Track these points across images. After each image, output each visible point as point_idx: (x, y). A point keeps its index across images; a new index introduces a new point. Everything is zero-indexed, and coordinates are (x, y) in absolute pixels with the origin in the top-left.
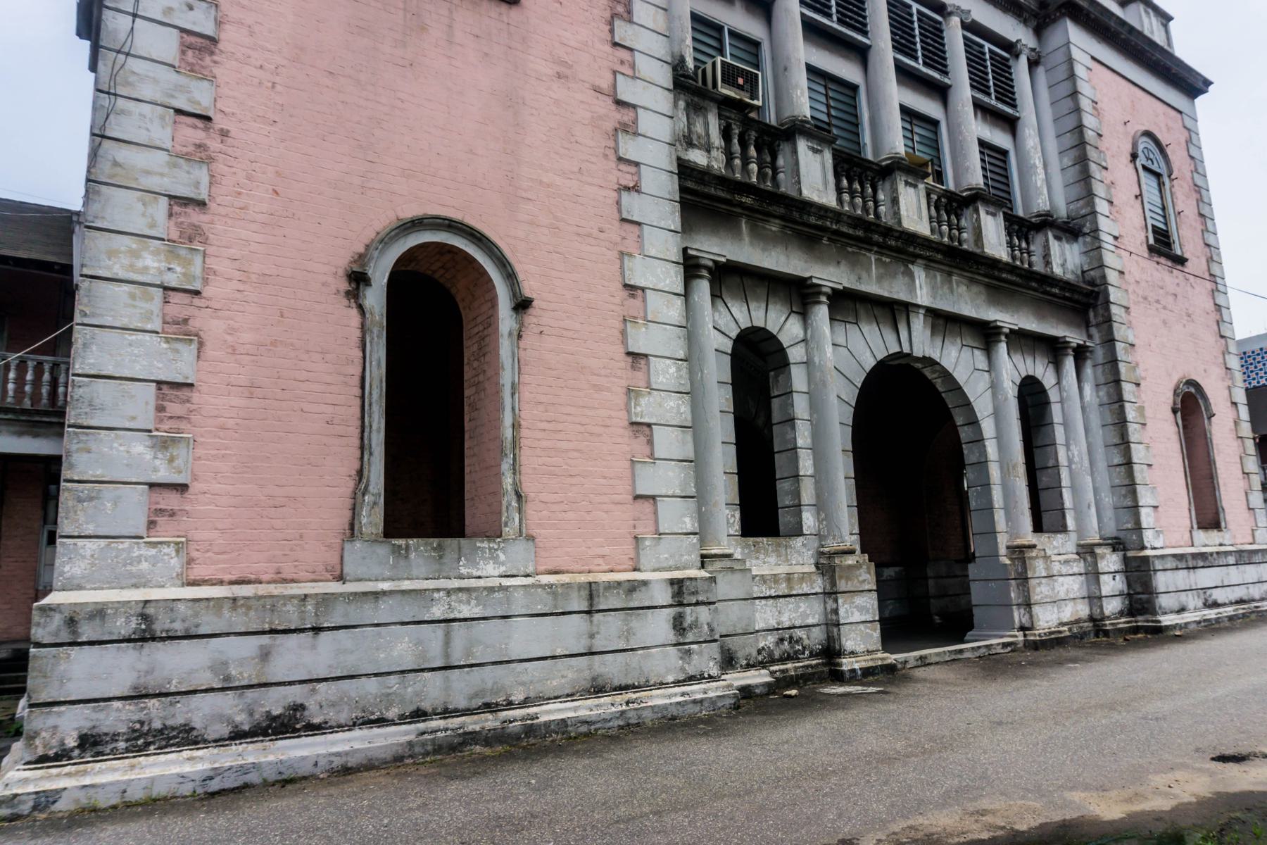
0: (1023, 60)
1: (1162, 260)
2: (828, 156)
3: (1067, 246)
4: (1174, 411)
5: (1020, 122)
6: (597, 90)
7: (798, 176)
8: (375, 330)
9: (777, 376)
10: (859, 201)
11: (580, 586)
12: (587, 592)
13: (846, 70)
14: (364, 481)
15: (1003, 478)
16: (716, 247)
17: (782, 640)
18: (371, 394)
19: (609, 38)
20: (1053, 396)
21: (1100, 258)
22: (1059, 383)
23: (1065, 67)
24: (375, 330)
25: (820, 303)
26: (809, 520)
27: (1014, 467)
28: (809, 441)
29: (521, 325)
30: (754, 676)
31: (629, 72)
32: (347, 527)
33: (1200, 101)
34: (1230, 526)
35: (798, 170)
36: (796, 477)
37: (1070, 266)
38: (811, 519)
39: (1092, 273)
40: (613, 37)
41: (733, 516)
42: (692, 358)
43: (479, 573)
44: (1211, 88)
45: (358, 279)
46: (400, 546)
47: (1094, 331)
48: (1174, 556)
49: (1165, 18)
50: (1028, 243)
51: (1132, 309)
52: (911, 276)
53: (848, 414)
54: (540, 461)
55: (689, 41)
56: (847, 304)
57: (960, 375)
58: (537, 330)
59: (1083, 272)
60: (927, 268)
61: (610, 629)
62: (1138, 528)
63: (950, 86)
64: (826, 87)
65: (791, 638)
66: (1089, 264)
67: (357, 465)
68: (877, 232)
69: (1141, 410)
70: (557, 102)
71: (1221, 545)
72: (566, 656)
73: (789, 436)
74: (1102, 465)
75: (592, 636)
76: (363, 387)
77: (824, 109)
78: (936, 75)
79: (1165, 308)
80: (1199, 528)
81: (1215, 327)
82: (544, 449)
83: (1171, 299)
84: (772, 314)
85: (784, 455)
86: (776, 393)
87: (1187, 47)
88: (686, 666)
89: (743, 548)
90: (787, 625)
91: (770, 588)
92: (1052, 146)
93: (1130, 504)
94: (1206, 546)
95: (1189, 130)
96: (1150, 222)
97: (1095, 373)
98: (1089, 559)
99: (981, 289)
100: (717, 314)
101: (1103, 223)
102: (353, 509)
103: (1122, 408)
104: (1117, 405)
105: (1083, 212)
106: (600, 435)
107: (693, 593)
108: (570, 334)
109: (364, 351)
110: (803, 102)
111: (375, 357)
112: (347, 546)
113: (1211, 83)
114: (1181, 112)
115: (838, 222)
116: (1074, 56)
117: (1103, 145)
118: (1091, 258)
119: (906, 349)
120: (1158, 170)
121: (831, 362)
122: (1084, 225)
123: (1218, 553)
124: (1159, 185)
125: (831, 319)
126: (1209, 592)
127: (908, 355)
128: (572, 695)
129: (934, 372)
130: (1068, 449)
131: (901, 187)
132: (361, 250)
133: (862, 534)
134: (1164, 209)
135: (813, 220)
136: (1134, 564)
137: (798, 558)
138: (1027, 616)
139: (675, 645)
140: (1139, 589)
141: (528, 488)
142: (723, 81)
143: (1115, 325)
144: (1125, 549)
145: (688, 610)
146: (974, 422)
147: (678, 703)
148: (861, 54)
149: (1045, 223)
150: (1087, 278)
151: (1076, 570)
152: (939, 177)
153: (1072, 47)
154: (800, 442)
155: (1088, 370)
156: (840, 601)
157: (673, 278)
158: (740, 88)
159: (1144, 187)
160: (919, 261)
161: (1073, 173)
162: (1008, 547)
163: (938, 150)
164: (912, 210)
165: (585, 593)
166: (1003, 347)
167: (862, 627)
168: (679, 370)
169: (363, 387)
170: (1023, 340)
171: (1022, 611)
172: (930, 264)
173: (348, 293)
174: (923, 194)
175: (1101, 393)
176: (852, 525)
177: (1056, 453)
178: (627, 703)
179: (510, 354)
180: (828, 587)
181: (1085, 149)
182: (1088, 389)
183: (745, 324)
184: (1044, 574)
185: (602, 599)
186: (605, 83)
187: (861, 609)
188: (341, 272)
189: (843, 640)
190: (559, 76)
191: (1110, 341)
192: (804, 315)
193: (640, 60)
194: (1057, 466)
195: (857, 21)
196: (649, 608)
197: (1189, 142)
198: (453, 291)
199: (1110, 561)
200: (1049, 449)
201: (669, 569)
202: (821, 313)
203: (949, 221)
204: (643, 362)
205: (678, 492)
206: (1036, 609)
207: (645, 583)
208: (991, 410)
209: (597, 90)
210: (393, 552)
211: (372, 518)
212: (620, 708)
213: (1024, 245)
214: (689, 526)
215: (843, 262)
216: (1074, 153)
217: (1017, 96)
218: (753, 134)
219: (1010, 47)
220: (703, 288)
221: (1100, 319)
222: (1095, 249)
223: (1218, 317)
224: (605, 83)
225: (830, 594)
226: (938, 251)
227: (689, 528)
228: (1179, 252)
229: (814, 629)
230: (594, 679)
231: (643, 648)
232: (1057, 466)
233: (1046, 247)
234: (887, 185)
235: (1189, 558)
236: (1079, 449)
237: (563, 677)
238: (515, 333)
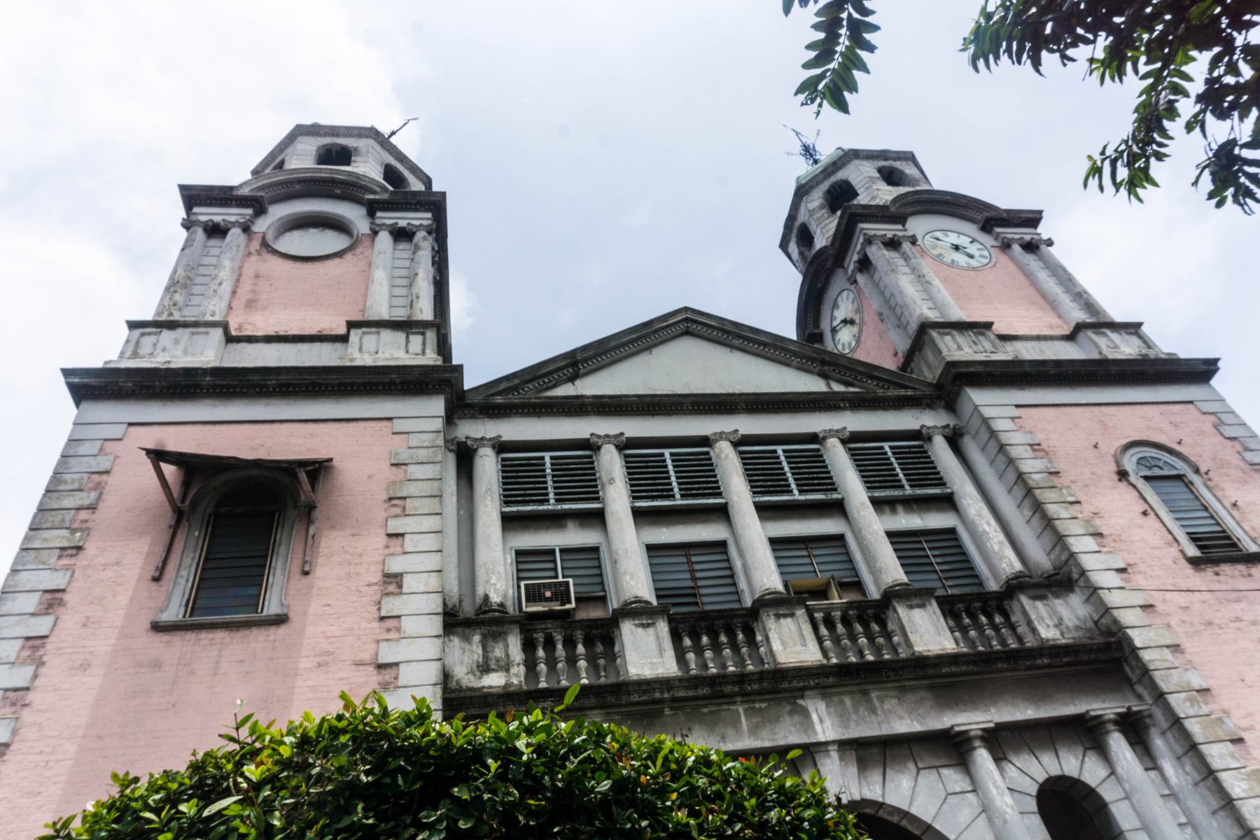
5: (956, 496)
20: (1109, 793)
23: (983, 429)
33: (1214, 382)
39: (1103, 621)
44: (1220, 364)
47: (1139, 689)
49: (1133, 328)
51: (1187, 644)
52: (805, 713)
59: (1096, 623)
60: (824, 696)
63: (952, 493)
66: (1096, 611)
68: (727, 683)
70: (313, 688)
87: (1172, 340)
97: (1167, 741)
99: (923, 694)
105: (1064, 557)
113: (1217, 360)
114: (1191, 402)
115: (669, 689)
116: (986, 415)
118: (1093, 604)
120: (1174, 472)
124: (1187, 486)
134: (1206, 509)
135: (635, 698)
155: (1158, 743)
158: (547, 600)
160: (807, 693)
172: (824, 692)
181: (1033, 495)
183: (1041, 777)
191: (1160, 697)
202: (982, 758)
216: (1027, 503)
218: (579, 635)
221: (1138, 672)
222: (1093, 592)
226: (827, 676)
233: (1025, 613)
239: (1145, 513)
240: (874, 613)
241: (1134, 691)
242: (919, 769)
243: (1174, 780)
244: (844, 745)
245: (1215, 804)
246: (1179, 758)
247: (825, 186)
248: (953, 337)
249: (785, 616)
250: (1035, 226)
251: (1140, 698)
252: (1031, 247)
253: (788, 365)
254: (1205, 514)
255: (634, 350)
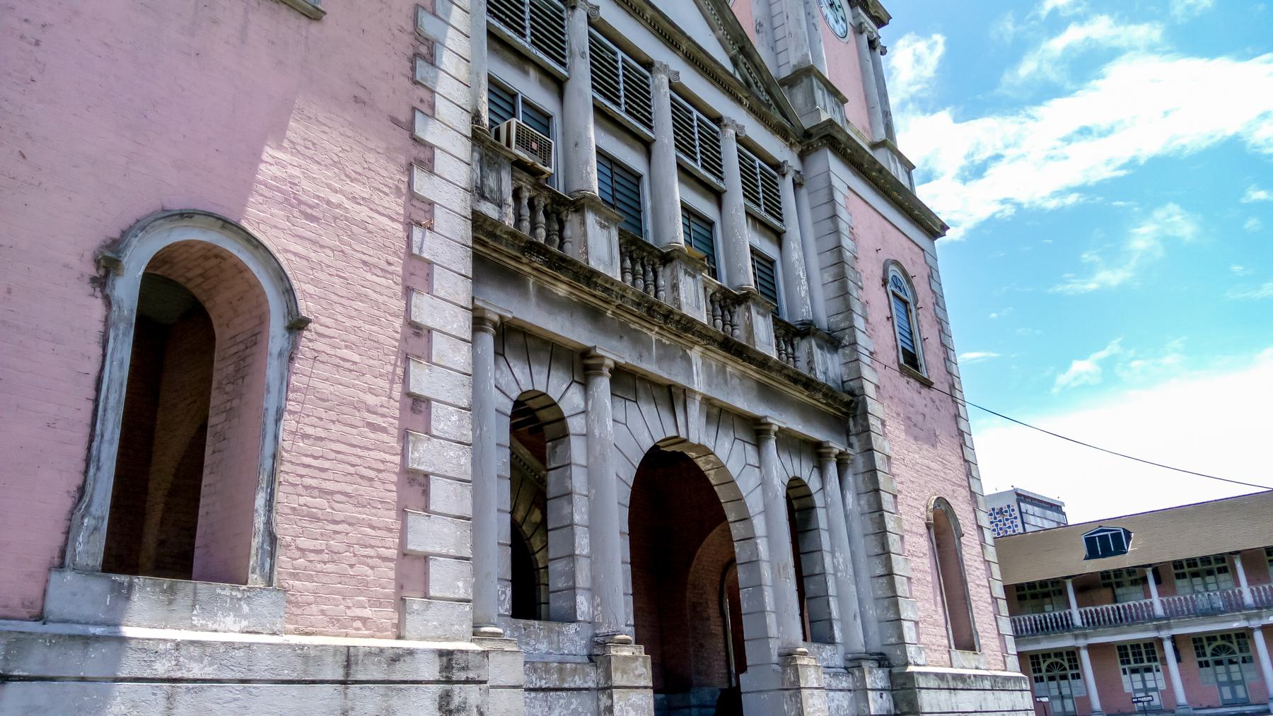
0: (789, 179)
1: (912, 380)
2: (614, 233)
3: (828, 356)
4: (928, 526)
6: (395, 121)
7: (586, 247)
8: (122, 326)
9: (554, 447)
10: (640, 282)
11: (336, 649)
12: (344, 658)
13: (631, 158)
14: (86, 499)
15: (773, 580)
16: (504, 304)
18: (107, 397)
20: (818, 500)
22: (823, 488)
23: (825, 191)
24: (122, 326)
25: (601, 375)
26: (583, 605)
27: (785, 567)
29: (294, 346)
31: (428, 111)
32: (56, 553)
33: (938, 242)
35: (586, 241)
36: (572, 556)
37: (831, 374)
38: (585, 604)
41: (504, 592)
42: (475, 408)
43: (215, 626)
44: (947, 232)
45: (107, 265)
46: (121, 584)
47: (853, 439)
48: (936, 674)
49: (909, 167)
53: (625, 495)
54: (302, 500)
57: (734, 468)
58: (309, 354)
59: (843, 382)
62: (901, 642)
67: (79, 481)
73: (566, 511)
74: (864, 575)
76: (98, 389)
80: (957, 648)
82: (306, 487)
83: (920, 418)
85: (557, 532)
86: (553, 465)
92: (815, 263)
98: (857, 673)
100: (498, 373)
101: (861, 339)
102: (68, 533)
106: (371, 479)
107: (463, 669)
108: (347, 365)
109: (104, 347)
110: (592, 181)
111: (118, 356)
112: (55, 577)
119: (683, 435)
121: (609, 441)
122: (843, 338)
123: (975, 676)
127: (684, 441)
129: (707, 462)
130: (833, 556)
131: (681, 274)
132: (117, 235)
134: (911, 334)
136: (900, 681)
137: (573, 640)
141: (284, 529)
142: (517, 142)
145: (456, 687)
146: (745, 519)
149: (806, 330)
152: (714, 273)
154: (577, 518)
155: (850, 479)
156: (615, 697)
157: (461, 323)
158: (532, 151)
161: (833, 289)
163: (713, 249)
164: (690, 296)
165: (341, 659)
166: (772, 444)
168: (460, 420)
169: (98, 389)
170: (792, 443)
173: (94, 280)
174: (700, 285)
176: (627, 615)
179: (277, 376)
180: (602, 681)
182: (850, 498)
183: (526, 386)
184: (816, 685)
186: (403, 116)
188: (89, 255)
191: (869, 450)
192: (585, 385)
193: (440, 104)
197: (930, 277)
198: (207, 305)
199: (875, 678)
200: (815, 555)
201: (433, 639)
202: (603, 385)
203: (723, 316)
204: (424, 405)
205: (452, 552)
207: (411, 652)
208: (761, 508)
209: (395, 121)
210: (112, 591)
211: (91, 545)
213: (790, 350)
215: (625, 338)
216: (834, 270)
217: (783, 211)
219: (777, 166)
220: (488, 340)
224: (403, 116)
227: (461, 594)
232: (823, 574)
233: (810, 354)
234: (668, 271)
235: (950, 678)
236: (843, 557)
238: (287, 354)
240: (562, 207)
243: (850, 506)
244: (708, 401)
245: (870, 529)
249: (690, 275)
250: (879, 27)
251: (850, 445)
252: (872, 44)
255: (708, 13)
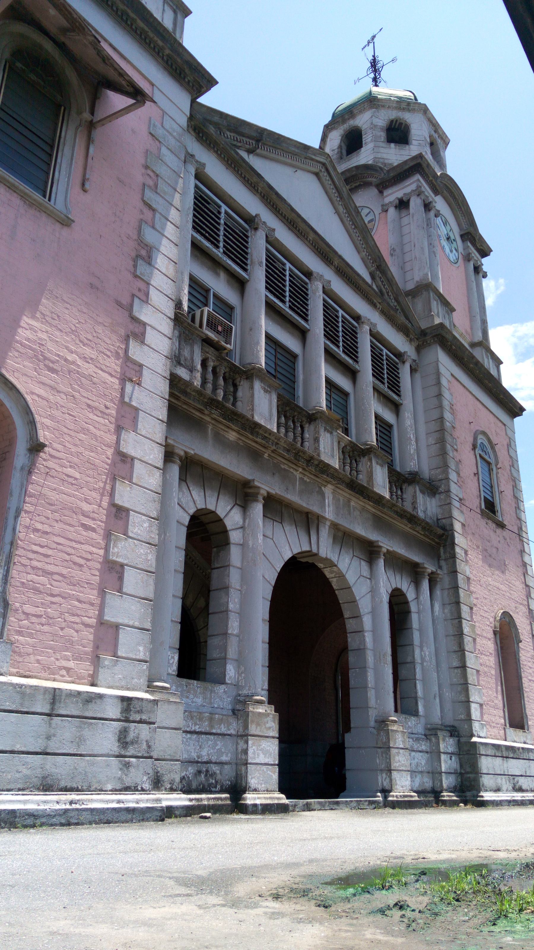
1: (490, 522)
3: (428, 499)
6: (119, 304)
10: (291, 434)
12: (51, 696)
16: (189, 444)
17: (200, 772)
19: (132, 271)
20: (413, 607)
21: (450, 511)
22: (417, 598)
26: (231, 671)
28: (238, 606)
30: (175, 799)
31: (144, 298)
33: (517, 420)
34: (530, 730)
37: (429, 513)
38: (233, 671)
39: (444, 521)
40: (135, 270)
47: (443, 563)
48: (494, 745)
50: (402, 492)
54: (30, 577)
55: (186, 291)
56: (275, 508)
59: (438, 520)
61: (65, 732)
64: (275, 350)
65: (207, 771)
69: (473, 627)
71: (525, 743)
72: (23, 753)
74: (444, 666)
75: (48, 738)
77: (273, 366)
78: (350, 361)
79: (490, 556)
81: (522, 578)
82: (33, 568)
83: (494, 550)
84: (221, 503)
88: (124, 777)
89: (177, 687)
90: (205, 759)
91: (196, 724)
92: (422, 429)
93: (463, 699)
94: (515, 742)
95: (510, 438)
96: (483, 494)
98: (434, 739)
101: (454, 488)
103: (460, 623)
104: (457, 621)
105: (440, 477)
107: (138, 712)
108: (70, 480)
114: (505, 425)
117: (456, 434)
119: (315, 550)
120: (489, 460)
121: (260, 553)
122: (440, 487)
123: (523, 748)
124: (489, 470)
125: (264, 516)
126: (517, 779)
127: (316, 555)
128: (23, 790)
129: (331, 572)
130: (422, 650)
131: (322, 431)
133: (269, 690)
134: (492, 487)
136: (466, 748)
138: (388, 780)
139: (117, 756)
140: (469, 770)
143: (458, 560)
144: (458, 736)
147: (114, 809)
148: (303, 334)
150: (440, 524)
151: (424, 748)
152: (346, 431)
153: (440, 364)
154: (231, 606)
155: (438, 592)
156: (250, 742)
157: (156, 456)
158: (218, 332)
159: (480, 469)
162: (376, 721)
164: (328, 449)
165: (49, 697)
166: (381, 562)
167: (264, 768)
168: (150, 526)
170: (395, 562)
171: (384, 775)
175: (446, 611)
177: (413, 652)
178: (71, 803)
180: (241, 730)
181: (444, 434)
185: (62, 705)
186: (125, 300)
187: (265, 753)
189: (249, 777)
190: (92, 286)
191: (454, 572)
194: (413, 662)
195: (302, 311)
196: (100, 719)
199: (447, 744)
203: (351, 463)
204: (124, 514)
205: (137, 624)
206: (395, 774)
207: (101, 696)
208: (369, 609)
209: (119, 304)
212: (64, 807)
213: (399, 492)
214: (142, 654)
219: (399, 355)
220: (175, 470)
223: (525, 570)
224: (125, 300)
225: (242, 736)
228: (500, 519)
229: (226, 767)
230: (44, 778)
231: (90, 755)
233: (415, 497)
235: (504, 749)
237: (18, 772)
239: (475, 474)
241: (439, 563)
242: (354, 556)
244: (335, 526)
246: (444, 605)
247: (393, 114)
248: (437, 304)
249: (328, 431)
251: (440, 567)
252: (477, 269)
253: (359, 252)
254: (489, 488)
